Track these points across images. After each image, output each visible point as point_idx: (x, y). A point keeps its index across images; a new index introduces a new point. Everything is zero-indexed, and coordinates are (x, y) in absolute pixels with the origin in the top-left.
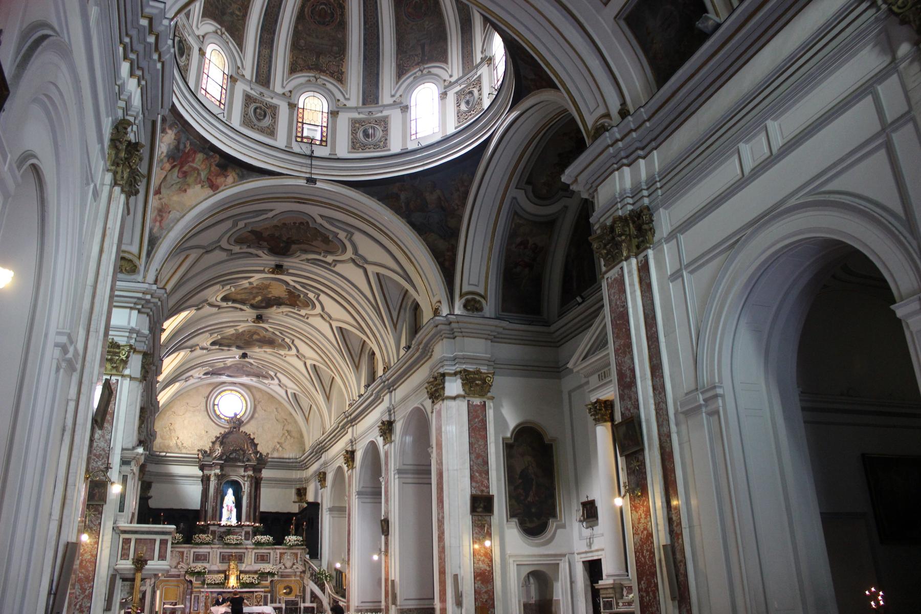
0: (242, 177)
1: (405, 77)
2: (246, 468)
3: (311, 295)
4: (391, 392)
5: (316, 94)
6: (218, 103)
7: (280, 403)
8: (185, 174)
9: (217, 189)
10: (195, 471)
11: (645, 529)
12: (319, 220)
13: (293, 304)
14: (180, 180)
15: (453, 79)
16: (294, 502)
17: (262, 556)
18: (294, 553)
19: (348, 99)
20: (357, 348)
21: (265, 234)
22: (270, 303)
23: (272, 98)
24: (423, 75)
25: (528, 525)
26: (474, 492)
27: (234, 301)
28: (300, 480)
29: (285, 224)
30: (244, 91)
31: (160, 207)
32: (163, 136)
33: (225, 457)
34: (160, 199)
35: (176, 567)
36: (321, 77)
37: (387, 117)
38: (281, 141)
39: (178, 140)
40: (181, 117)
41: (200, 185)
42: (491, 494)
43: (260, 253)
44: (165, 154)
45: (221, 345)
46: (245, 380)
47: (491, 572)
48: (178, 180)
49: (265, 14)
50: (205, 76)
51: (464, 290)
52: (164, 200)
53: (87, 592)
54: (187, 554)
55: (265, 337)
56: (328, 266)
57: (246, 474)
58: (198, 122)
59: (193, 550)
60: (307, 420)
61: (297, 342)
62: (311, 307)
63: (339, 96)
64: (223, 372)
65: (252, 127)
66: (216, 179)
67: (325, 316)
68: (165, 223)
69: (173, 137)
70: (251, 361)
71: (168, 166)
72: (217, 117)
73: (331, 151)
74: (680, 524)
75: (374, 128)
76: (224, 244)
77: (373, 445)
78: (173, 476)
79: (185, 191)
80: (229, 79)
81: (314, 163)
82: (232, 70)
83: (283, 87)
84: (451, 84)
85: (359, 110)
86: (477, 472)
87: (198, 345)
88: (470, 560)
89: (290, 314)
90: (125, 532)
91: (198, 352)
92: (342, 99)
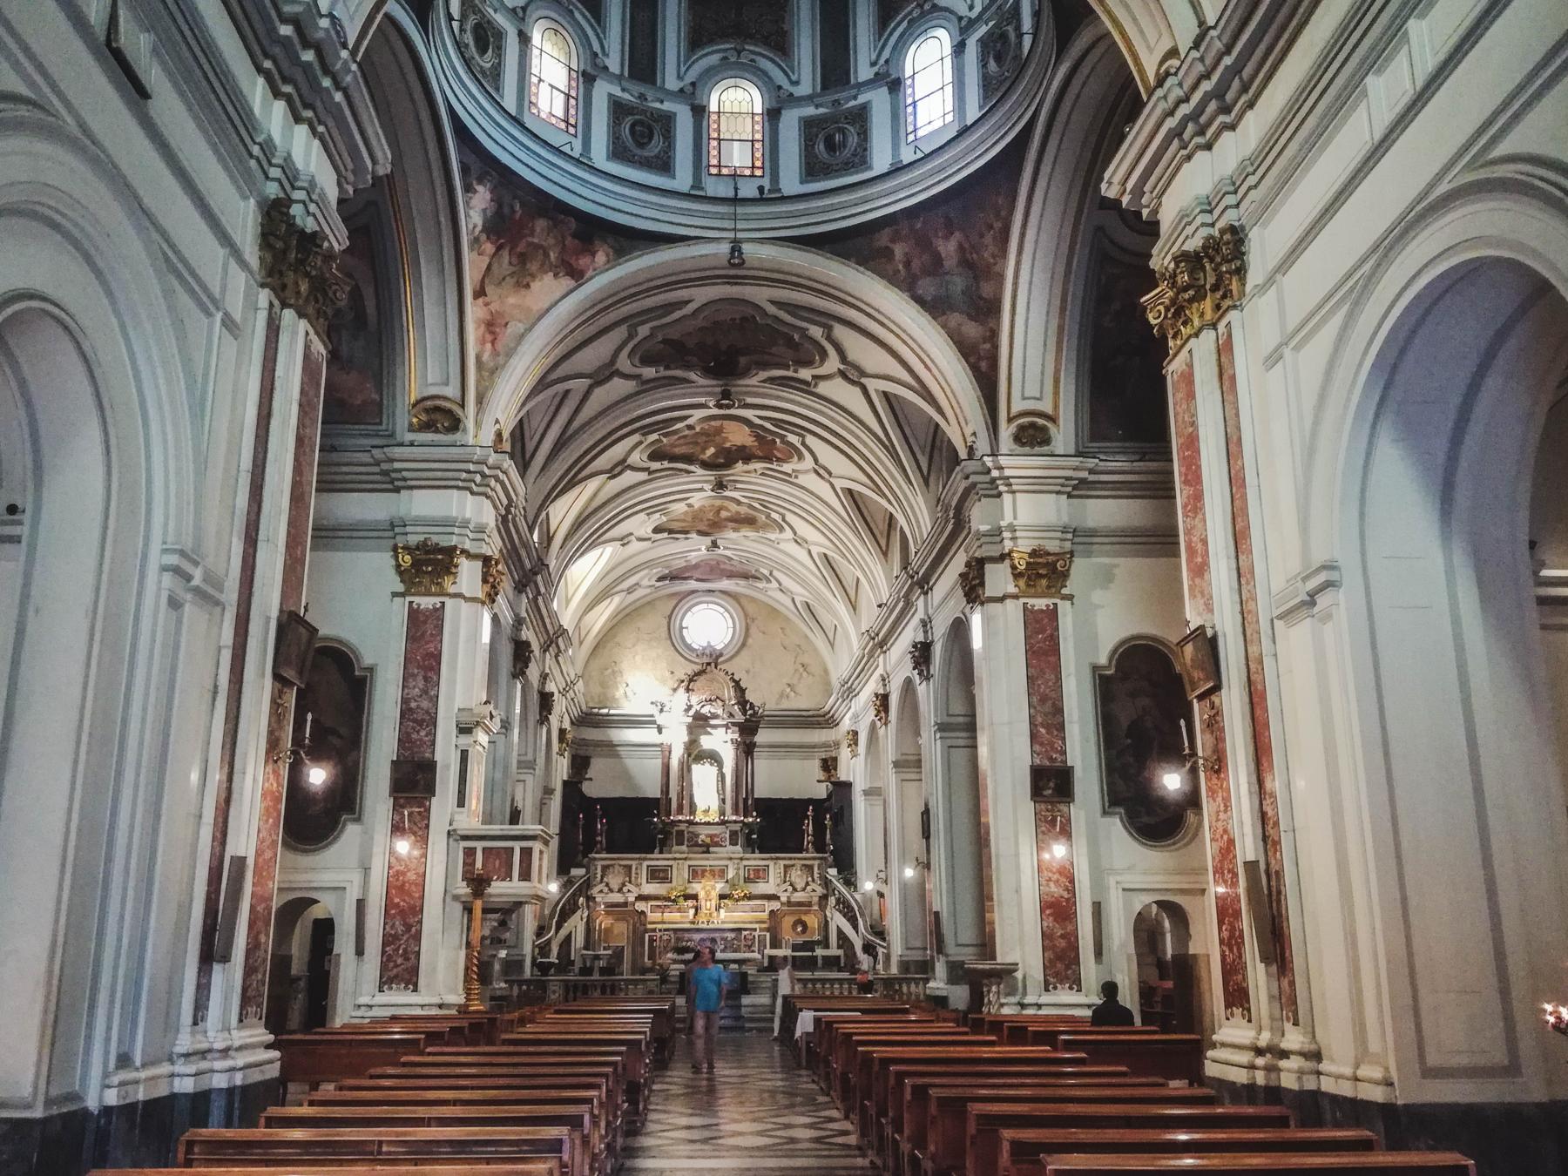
1: (710, 50)
6: (563, 125)
7: (787, 619)
8: (523, 259)
11: (1225, 831)
12: (772, 309)
13: (768, 458)
15: (974, 14)
19: (796, 83)
22: (729, 457)
23: (662, 102)
24: (923, 14)
25: (1145, 819)
26: (1038, 761)
27: (673, 458)
28: (826, 745)
30: (610, 95)
34: (486, 304)
36: (747, 47)
37: (869, 102)
38: (682, 179)
39: (497, 200)
40: (495, 161)
41: (551, 274)
43: (692, 376)
44: (479, 228)
45: (671, 531)
46: (726, 584)
47: (1071, 902)
48: (513, 269)
51: (1015, 410)
53: (414, 929)
55: (738, 513)
56: (805, 387)
58: (533, 169)
59: (645, 864)
60: (832, 645)
61: (790, 517)
67: (822, 472)
68: (499, 346)
69: (488, 196)
70: (728, 553)
71: (489, 248)
74: (1276, 824)
77: (908, 682)
79: (528, 286)
80: (581, 79)
81: (740, 210)
82: (585, 63)
83: (680, 77)
85: (816, 100)
86: (1042, 725)
87: (631, 534)
88: (1033, 879)
90: (466, 838)
91: (635, 546)
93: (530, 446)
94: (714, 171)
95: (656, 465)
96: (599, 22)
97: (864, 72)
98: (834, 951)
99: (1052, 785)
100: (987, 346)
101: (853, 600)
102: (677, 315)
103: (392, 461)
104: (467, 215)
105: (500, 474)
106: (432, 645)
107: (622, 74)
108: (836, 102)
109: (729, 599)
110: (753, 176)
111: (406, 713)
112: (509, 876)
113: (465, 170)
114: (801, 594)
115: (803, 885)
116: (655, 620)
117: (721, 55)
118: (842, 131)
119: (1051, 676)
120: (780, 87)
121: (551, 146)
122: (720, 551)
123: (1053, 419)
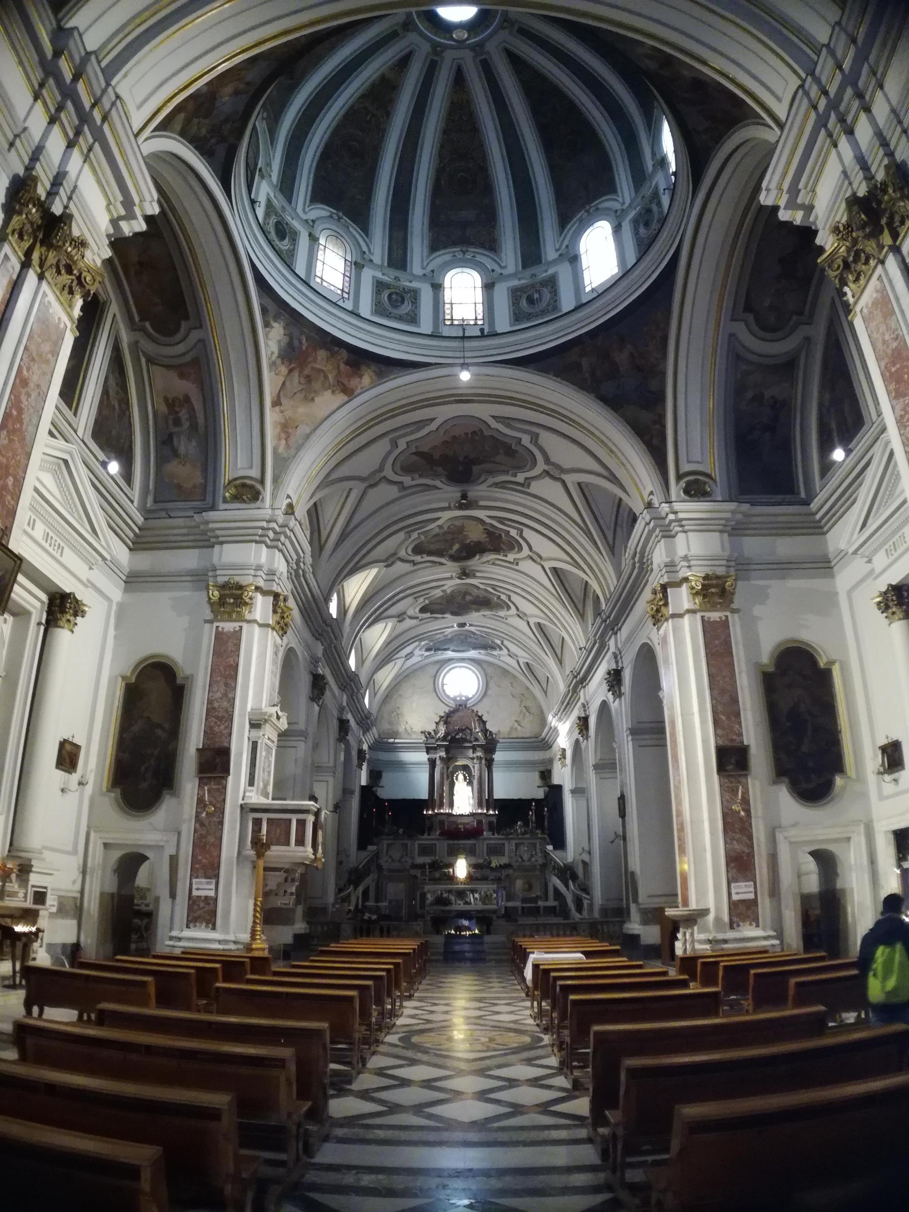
0: (381, 376)
2: (474, 748)
3: (513, 533)
4: (616, 633)
6: (339, 292)
7: (514, 676)
8: (309, 379)
10: (423, 757)
12: (494, 424)
13: (497, 550)
16: (539, 787)
19: (505, 267)
20: (578, 592)
21: (437, 455)
22: (470, 551)
26: (720, 743)
27: (430, 553)
29: (454, 437)
30: (374, 277)
31: (283, 421)
33: (449, 738)
34: (282, 412)
35: (400, 861)
38: (426, 326)
39: (290, 336)
41: (330, 391)
42: (745, 743)
43: (437, 483)
44: (276, 354)
46: (472, 654)
47: (751, 855)
55: (478, 597)
57: (475, 755)
60: (546, 693)
61: (514, 598)
62: (516, 549)
63: (490, 264)
64: (446, 647)
65: (388, 316)
67: (535, 557)
68: (292, 440)
69: (282, 331)
70: (472, 629)
71: (284, 370)
75: (539, 292)
76: (388, 472)
78: (406, 764)
79: (313, 399)
80: (353, 266)
83: (423, 268)
89: (497, 562)
92: (496, 267)
93: (324, 534)
94: (448, 323)
95: (418, 558)
96: (367, 236)
98: (551, 903)
101: (559, 656)
103: (207, 523)
104: (267, 345)
105: (288, 531)
106: (232, 659)
107: (383, 263)
108: (534, 275)
110: (476, 324)
111: (210, 711)
112: (287, 843)
113: (264, 311)
114: (523, 657)
116: (424, 680)
118: (539, 292)
122: (467, 628)
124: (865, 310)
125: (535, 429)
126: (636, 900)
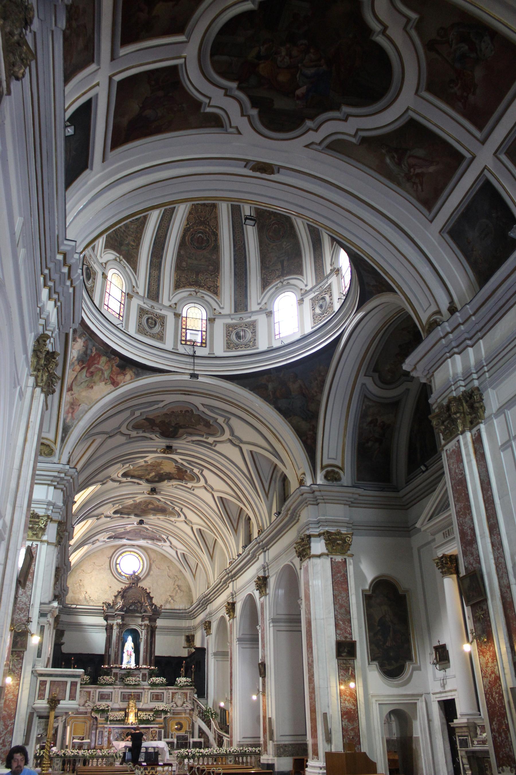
0: (137, 375)
5: (196, 305)
6: (117, 316)
7: (171, 561)
8: (92, 374)
9: (118, 385)
10: (100, 620)
11: (493, 672)
12: (201, 408)
13: (181, 479)
14: (88, 379)
15: (308, 288)
16: (184, 647)
17: (157, 696)
18: (184, 693)
19: (223, 308)
20: (235, 514)
21: (157, 421)
22: (162, 477)
23: (161, 310)
24: (283, 286)
26: (339, 639)
27: (133, 477)
28: (189, 628)
29: (173, 412)
30: (138, 305)
31: (72, 401)
32: (74, 344)
33: (125, 609)
34: (72, 395)
38: (169, 345)
39: (86, 346)
40: (88, 328)
41: (104, 383)
43: (153, 436)
44: (75, 358)
45: (122, 513)
46: (142, 542)
47: (356, 711)
49: (154, 244)
50: (107, 295)
51: (325, 463)
52: (74, 395)
54: (93, 693)
55: (158, 506)
56: (210, 446)
57: (143, 623)
59: (98, 690)
60: (194, 576)
61: (185, 510)
62: (196, 481)
64: (123, 536)
66: (117, 377)
67: (208, 488)
68: (76, 414)
69: (82, 344)
71: (78, 368)
72: (117, 327)
73: (210, 351)
76: (124, 429)
79: (92, 387)
81: (196, 361)
83: (170, 301)
84: (307, 292)
85: (232, 317)
87: (103, 514)
88: (337, 700)
91: (103, 520)
96: (136, 273)
97: (253, 306)
99: (346, 650)
100: (311, 433)
101: (211, 554)
102: (156, 406)
107: (144, 296)
109: (141, 550)
115: (181, 703)
117: (188, 293)
119: (344, 594)
120: (215, 309)
121: (113, 325)
123: (342, 469)
124: (448, 452)
125: (229, 416)
126: (271, 739)
